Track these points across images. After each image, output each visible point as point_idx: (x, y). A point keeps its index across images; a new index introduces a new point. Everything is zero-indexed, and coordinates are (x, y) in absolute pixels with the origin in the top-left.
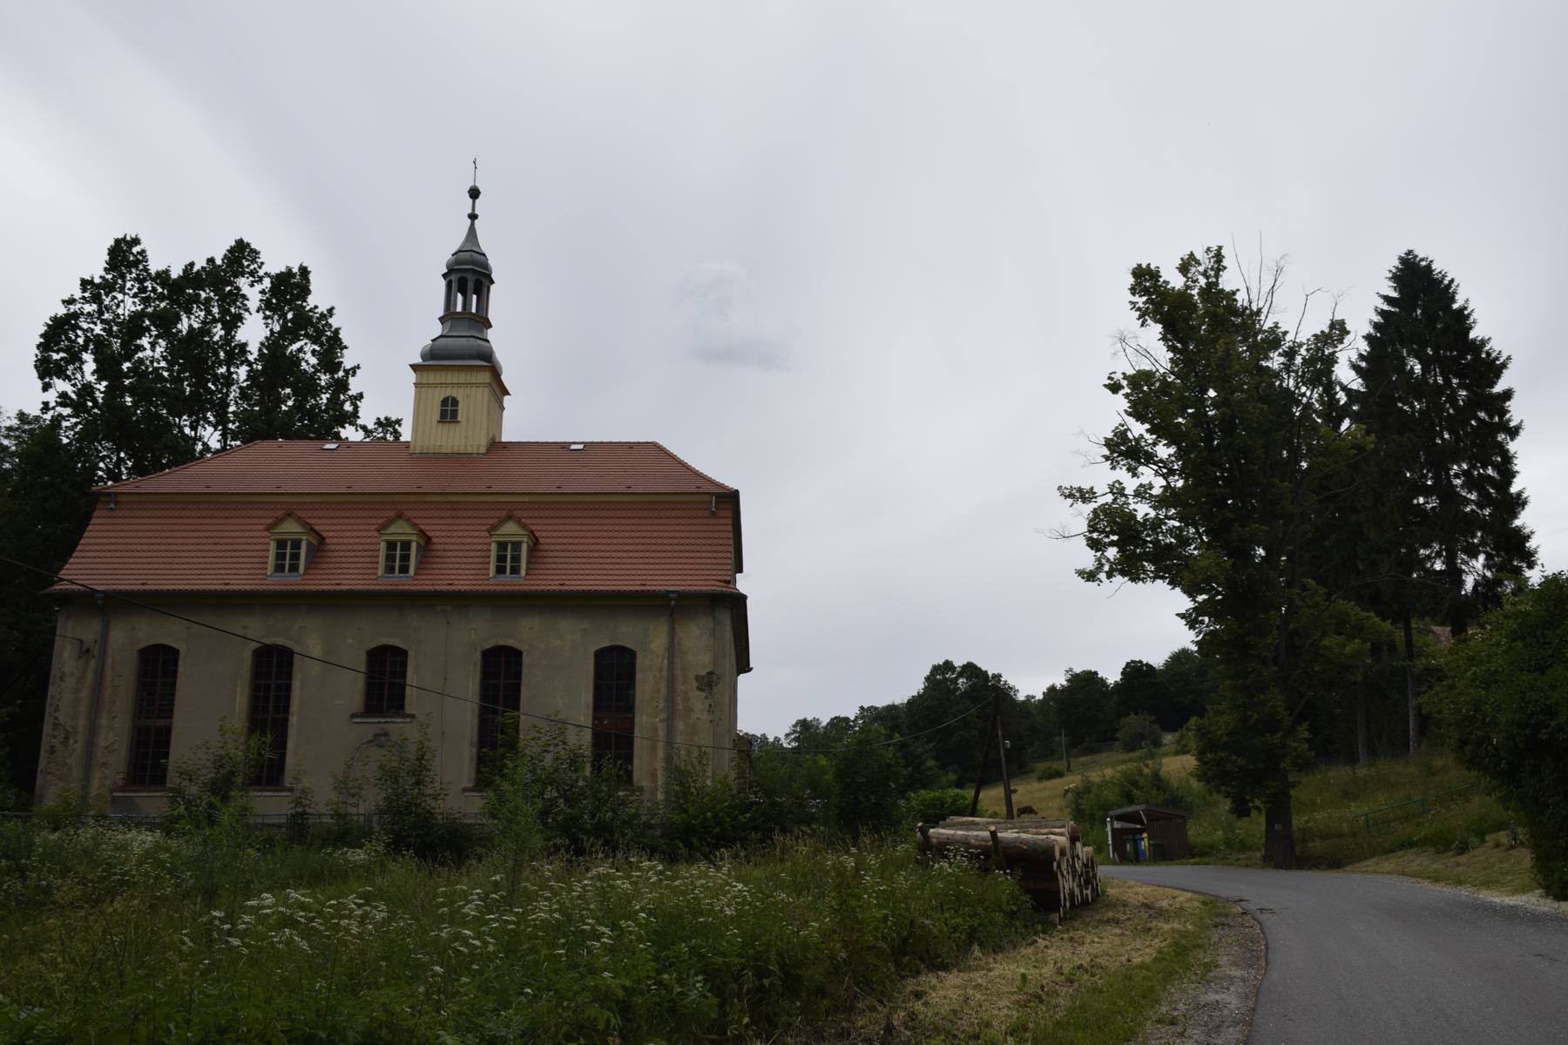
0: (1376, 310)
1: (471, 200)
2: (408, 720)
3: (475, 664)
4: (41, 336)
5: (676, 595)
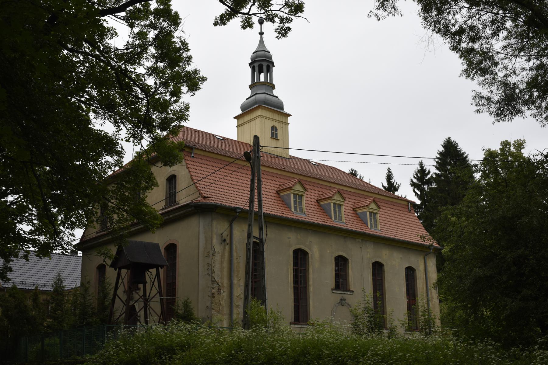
1: (260, 25)
2: (351, 293)
3: (370, 269)
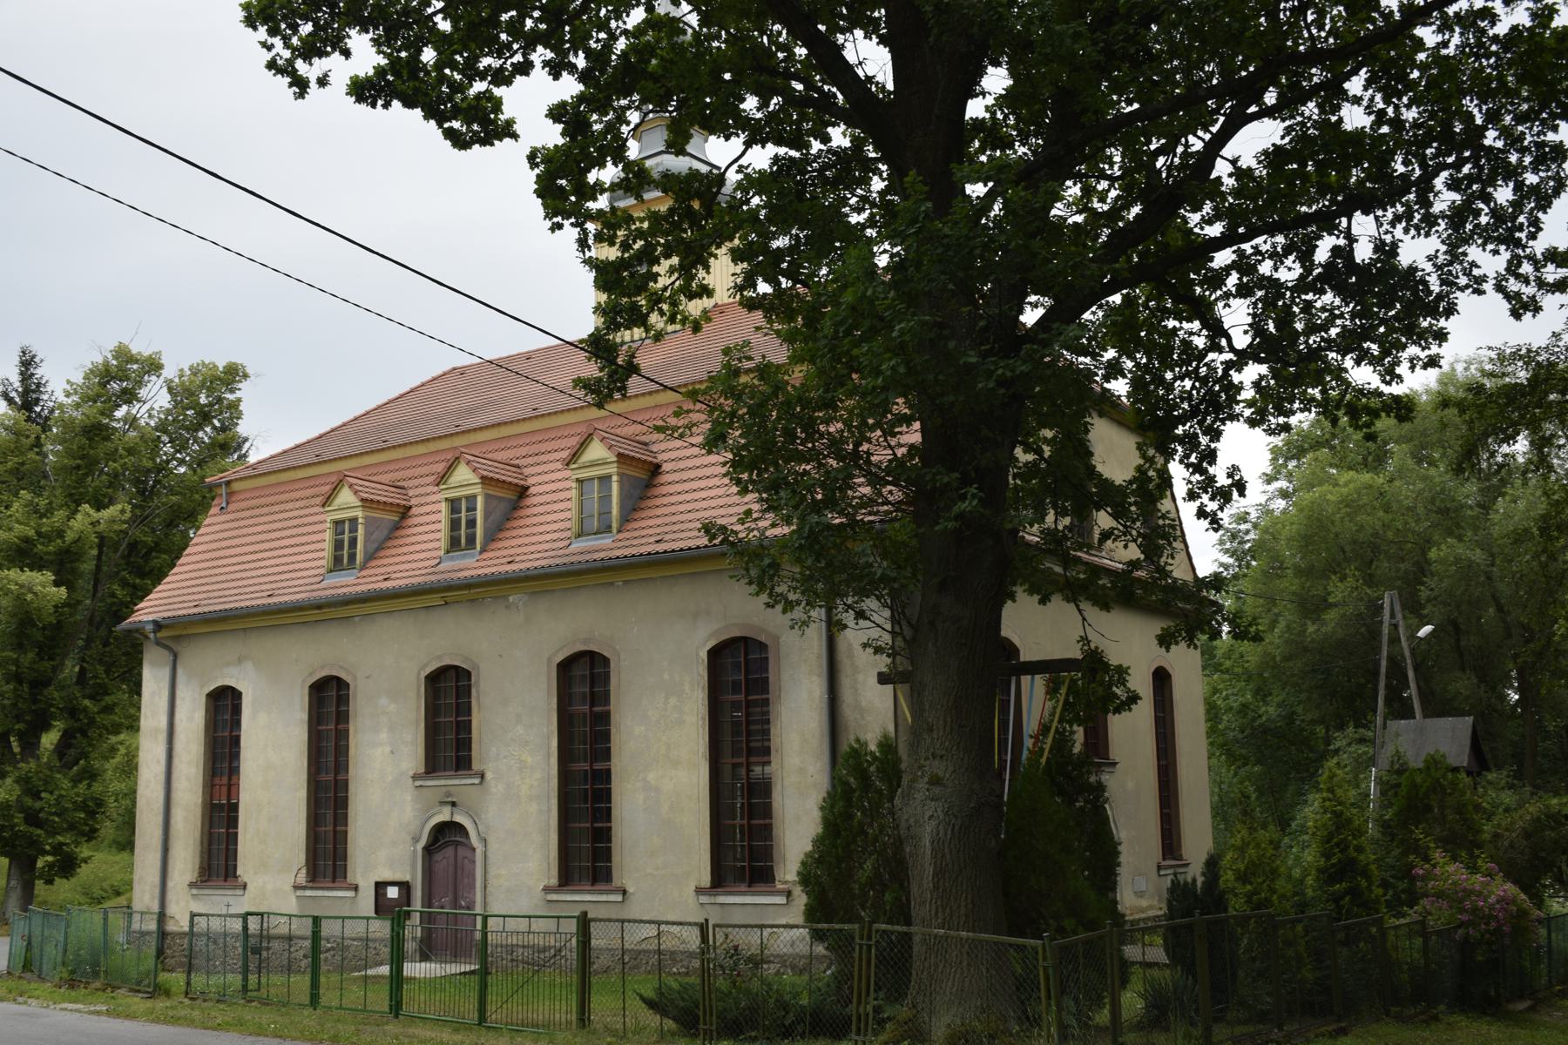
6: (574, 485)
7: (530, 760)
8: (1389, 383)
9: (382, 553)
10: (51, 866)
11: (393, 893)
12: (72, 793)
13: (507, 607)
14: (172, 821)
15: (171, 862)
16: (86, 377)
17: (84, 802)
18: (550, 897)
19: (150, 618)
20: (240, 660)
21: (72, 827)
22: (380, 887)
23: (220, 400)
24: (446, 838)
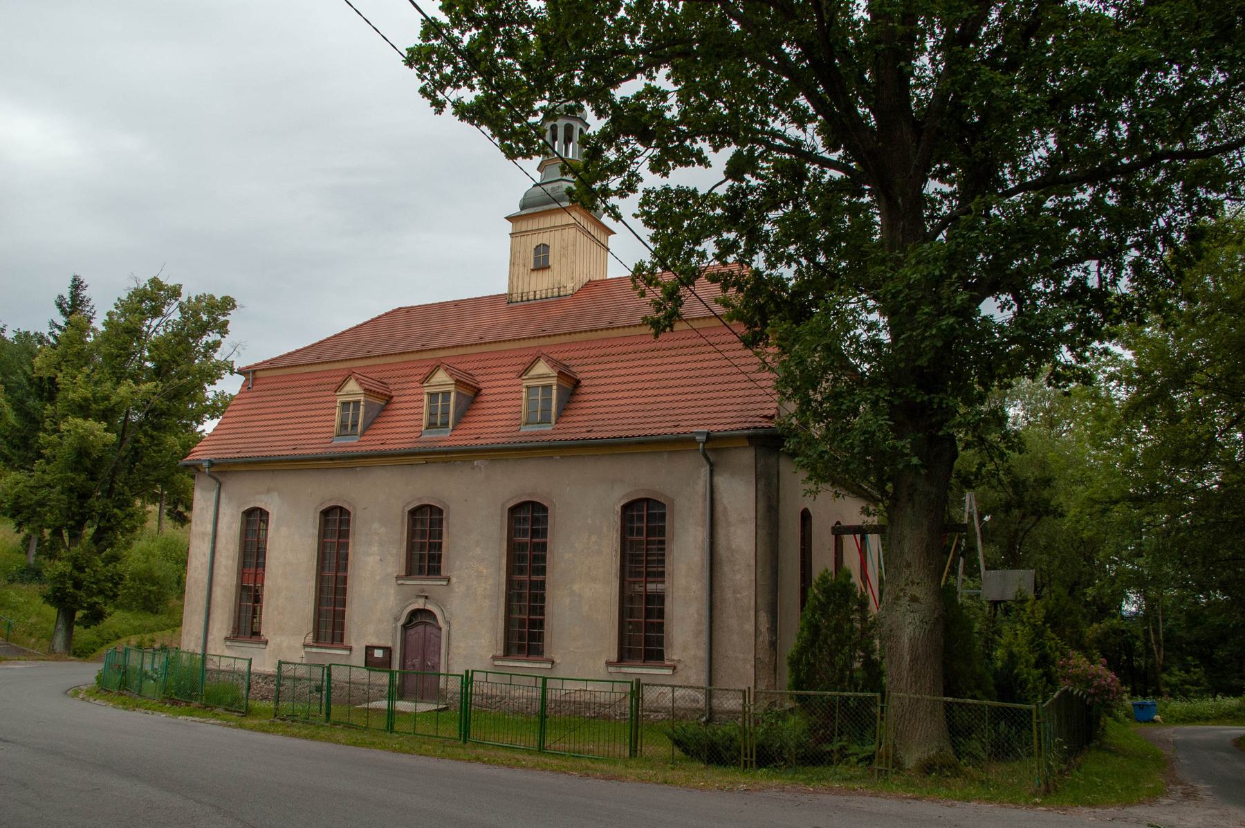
0: (60, 305)
4: (531, 158)
5: (704, 438)
6: (524, 390)
7: (485, 571)
8: (1081, 362)
9: (375, 426)
10: (85, 616)
11: (378, 654)
12: (104, 570)
13: (473, 468)
14: (213, 596)
15: (211, 623)
16: (130, 296)
17: (111, 576)
18: (496, 663)
19: (208, 458)
20: (269, 491)
21: (101, 592)
22: (369, 649)
23: (215, 320)
24: (419, 618)
